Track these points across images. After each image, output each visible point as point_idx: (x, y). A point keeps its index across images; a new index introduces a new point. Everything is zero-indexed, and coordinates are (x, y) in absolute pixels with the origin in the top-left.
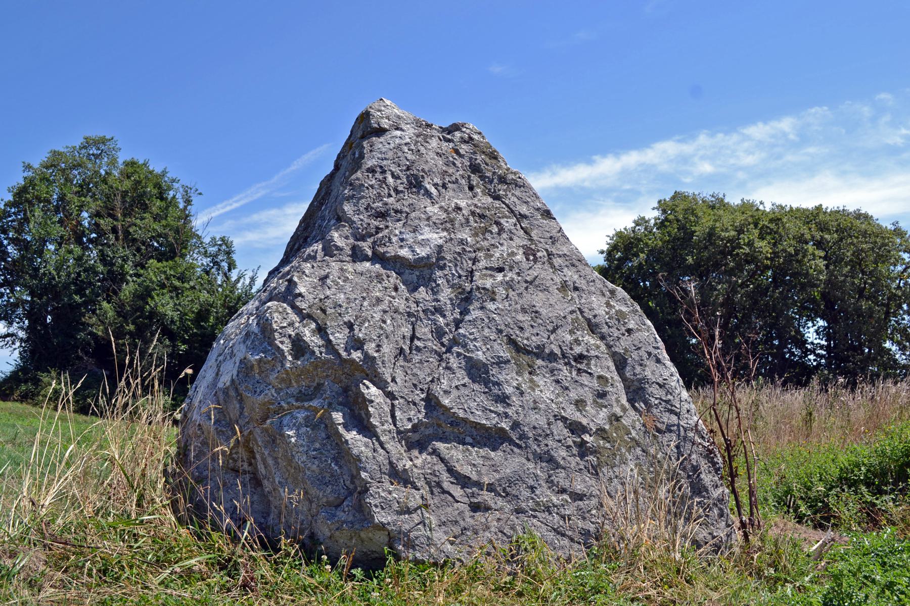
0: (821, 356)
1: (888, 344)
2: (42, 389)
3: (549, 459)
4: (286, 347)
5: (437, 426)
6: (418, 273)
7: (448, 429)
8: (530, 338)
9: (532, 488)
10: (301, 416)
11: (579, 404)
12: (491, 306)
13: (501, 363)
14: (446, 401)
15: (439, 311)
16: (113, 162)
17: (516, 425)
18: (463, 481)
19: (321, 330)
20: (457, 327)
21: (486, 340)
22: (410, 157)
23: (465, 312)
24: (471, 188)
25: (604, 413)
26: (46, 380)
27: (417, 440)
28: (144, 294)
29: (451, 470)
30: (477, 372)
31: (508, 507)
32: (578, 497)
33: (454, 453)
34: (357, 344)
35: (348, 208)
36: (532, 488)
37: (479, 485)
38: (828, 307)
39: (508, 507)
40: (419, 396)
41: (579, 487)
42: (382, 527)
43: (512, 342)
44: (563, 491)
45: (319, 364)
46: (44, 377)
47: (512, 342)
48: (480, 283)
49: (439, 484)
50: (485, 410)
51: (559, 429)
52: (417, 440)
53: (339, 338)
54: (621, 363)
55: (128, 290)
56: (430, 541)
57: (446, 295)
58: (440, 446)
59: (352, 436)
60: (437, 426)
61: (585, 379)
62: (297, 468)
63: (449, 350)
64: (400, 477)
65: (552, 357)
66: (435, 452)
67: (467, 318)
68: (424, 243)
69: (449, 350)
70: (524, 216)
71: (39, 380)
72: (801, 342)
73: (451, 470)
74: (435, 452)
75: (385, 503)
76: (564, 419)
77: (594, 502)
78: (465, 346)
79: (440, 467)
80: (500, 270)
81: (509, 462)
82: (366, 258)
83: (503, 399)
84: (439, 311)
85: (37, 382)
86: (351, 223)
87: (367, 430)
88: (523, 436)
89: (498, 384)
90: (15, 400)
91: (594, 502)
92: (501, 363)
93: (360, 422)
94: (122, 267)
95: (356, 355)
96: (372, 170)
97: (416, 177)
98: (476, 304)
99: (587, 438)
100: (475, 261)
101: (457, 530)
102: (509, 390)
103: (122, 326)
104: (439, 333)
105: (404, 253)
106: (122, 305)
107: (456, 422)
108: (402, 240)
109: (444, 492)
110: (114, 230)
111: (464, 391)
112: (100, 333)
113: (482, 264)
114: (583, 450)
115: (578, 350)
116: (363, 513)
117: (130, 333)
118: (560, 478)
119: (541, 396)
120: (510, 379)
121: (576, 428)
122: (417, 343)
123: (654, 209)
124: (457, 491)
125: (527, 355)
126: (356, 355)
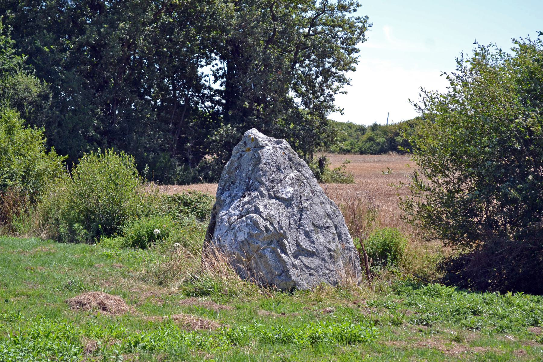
0: (218, 103)
1: (291, 94)
3: (324, 260)
4: (263, 229)
5: (301, 252)
6: (287, 202)
7: (301, 252)
8: (317, 223)
9: (322, 269)
10: (269, 250)
11: (329, 242)
12: (308, 213)
13: (312, 231)
14: (301, 244)
15: (294, 215)
17: (317, 250)
18: (307, 267)
19: (271, 224)
20: (300, 220)
21: (308, 224)
22: (275, 158)
23: (301, 215)
24: (291, 168)
25: (334, 245)
29: (304, 264)
31: (317, 275)
32: (331, 271)
33: (304, 259)
34: (281, 228)
35: (263, 179)
36: (322, 269)
37: (310, 268)
38: (236, 55)
39: (317, 275)
40: (294, 242)
41: (331, 268)
42: (293, 281)
43: (313, 224)
44: (327, 270)
45: (273, 234)
47: (313, 224)
48: (304, 205)
49: (302, 269)
50: (310, 246)
51: (326, 251)
53: (277, 226)
54: (336, 227)
56: (303, 285)
57: (296, 209)
58: (301, 257)
59: (283, 255)
60: (301, 252)
61: (329, 234)
62: (269, 265)
63: (299, 228)
64: (294, 266)
65: (321, 228)
66: (300, 259)
67: (303, 217)
68: (288, 192)
69: (299, 228)
70: (308, 178)
72: (195, 83)
73: (304, 264)
74: (300, 259)
76: (327, 247)
77: (335, 272)
78: (303, 226)
79: (302, 263)
80: (308, 200)
82: (273, 198)
83: (313, 242)
84: (294, 215)
86: (265, 185)
87: (286, 253)
88: (318, 254)
89: (312, 238)
91: (335, 272)
92: (312, 231)
93: (284, 252)
95: (282, 231)
96: (265, 164)
97: (278, 166)
98: (304, 212)
99: (332, 253)
100: (301, 197)
101: (308, 281)
102: (315, 239)
104: (296, 222)
105: (284, 196)
107: (304, 250)
108: (282, 191)
109: (303, 271)
111: (305, 240)
113: (303, 198)
114: (331, 257)
115: (327, 225)
116: (289, 278)
118: (327, 265)
119: (320, 238)
120: (314, 235)
121: (329, 250)
122: (291, 226)
124: (306, 270)
126: (282, 231)
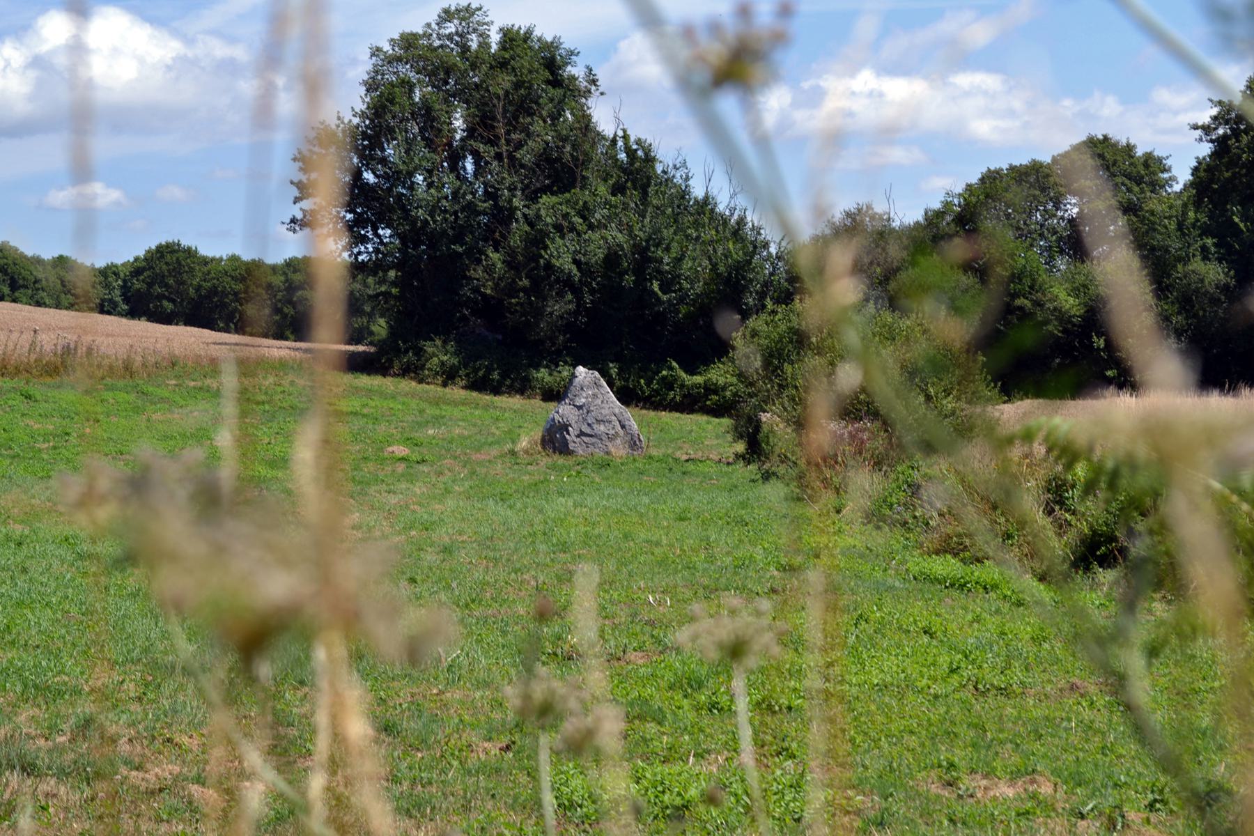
2: (427, 361)
6: (580, 408)
16: (484, 36)
26: (430, 350)
27: (578, 436)
28: (537, 240)
30: (589, 425)
46: (429, 348)
52: (578, 436)
55: (518, 229)
60: (582, 434)
71: (421, 349)
75: (571, 446)
81: (593, 440)
85: (419, 352)
90: (395, 375)
94: (510, 201)
103: (514, 281)
106: (512, 253)
110: (499, 157)
112: (489, 292)
117: (524, 290)
120: (595, 426)
123: (1195, 127)
125: (599, 422)
